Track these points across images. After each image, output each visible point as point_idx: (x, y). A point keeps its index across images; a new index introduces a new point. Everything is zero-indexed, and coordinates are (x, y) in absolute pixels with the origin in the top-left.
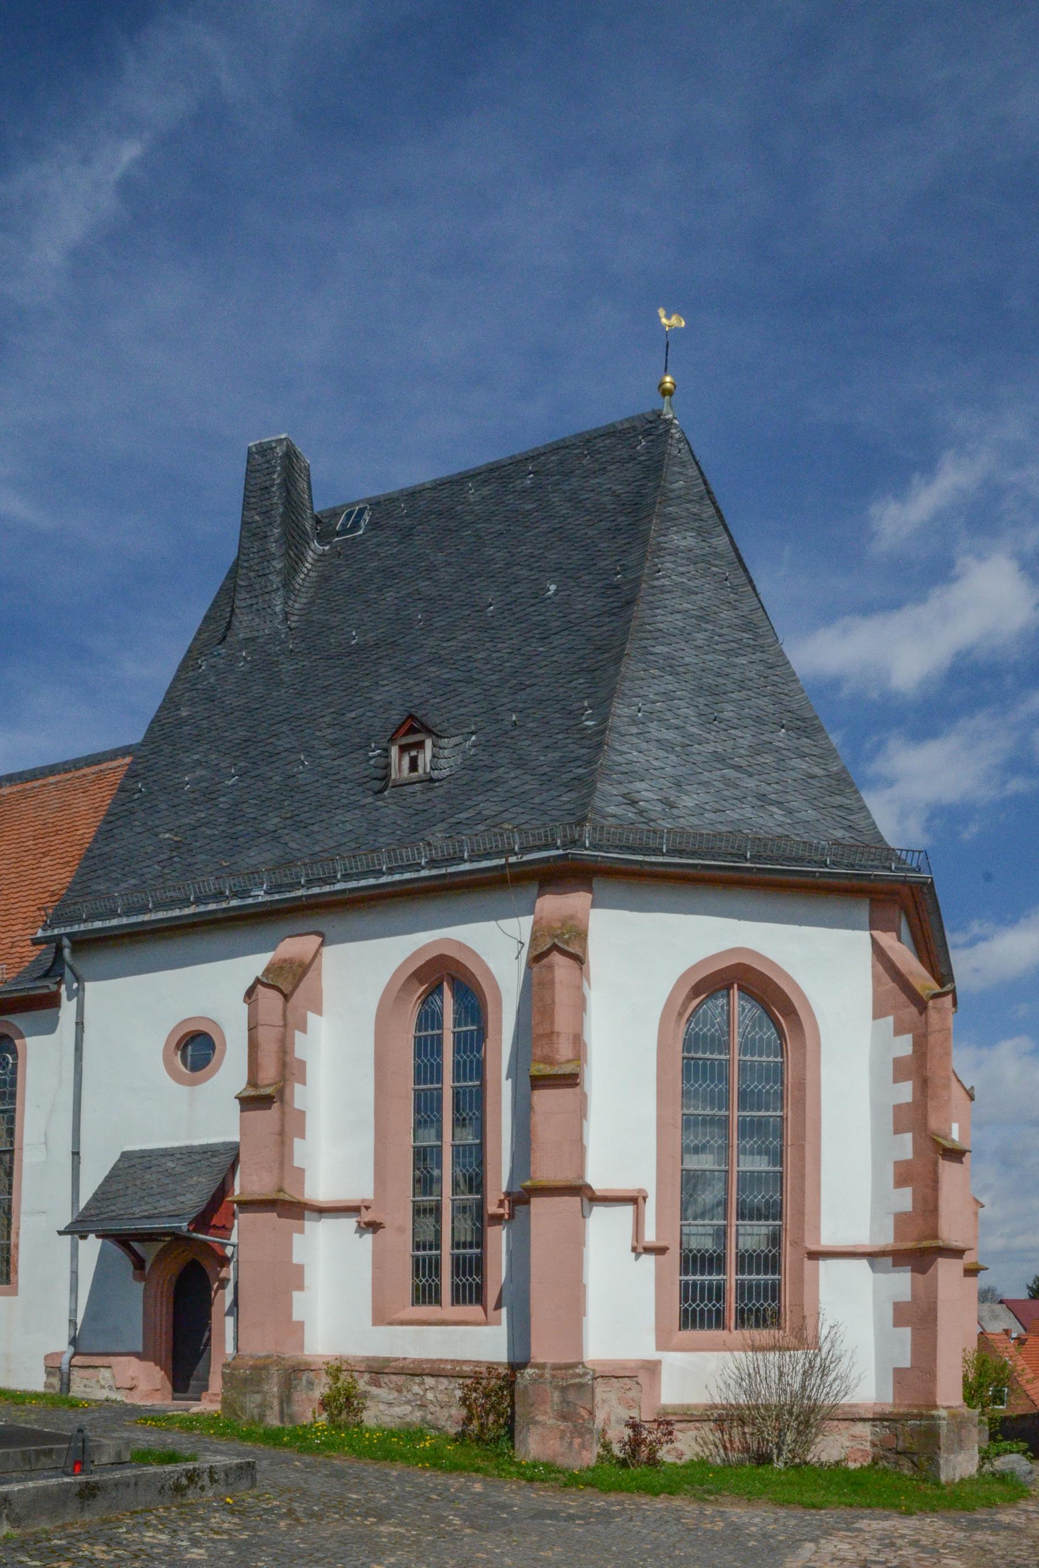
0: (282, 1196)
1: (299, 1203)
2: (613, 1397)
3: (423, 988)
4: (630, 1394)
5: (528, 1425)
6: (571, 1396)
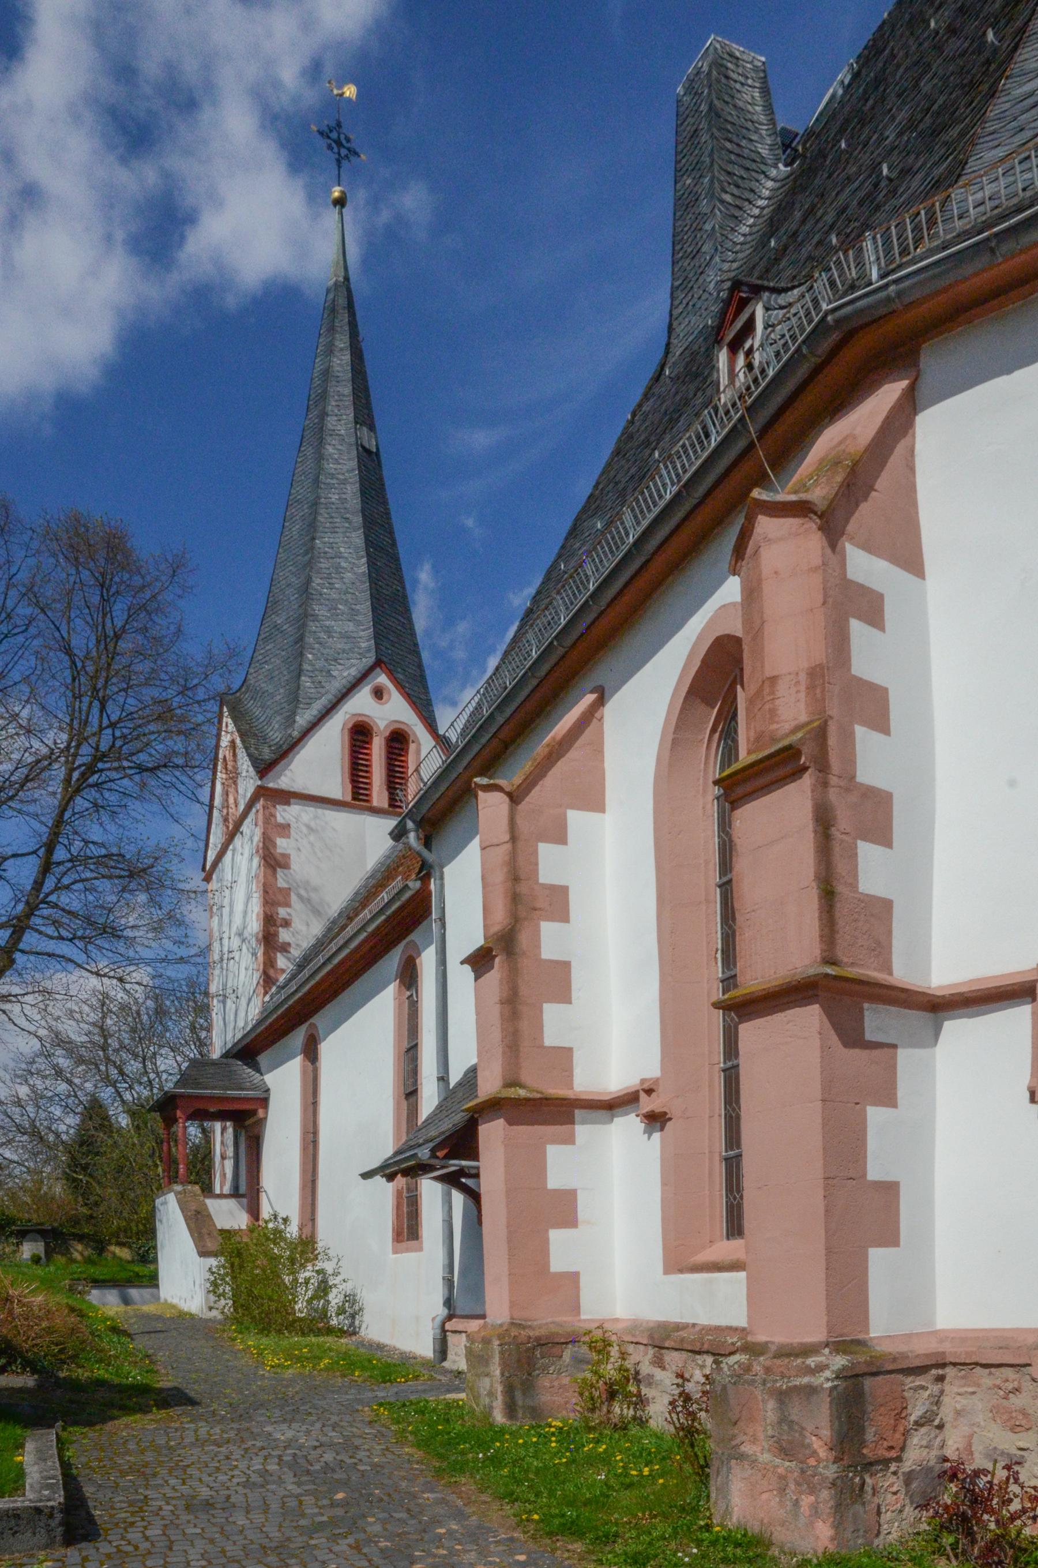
1: (546, 1099)
2: (978, 1405)
4: (1016, 1401)
5: (729, 1460)
6: (795, 1412)
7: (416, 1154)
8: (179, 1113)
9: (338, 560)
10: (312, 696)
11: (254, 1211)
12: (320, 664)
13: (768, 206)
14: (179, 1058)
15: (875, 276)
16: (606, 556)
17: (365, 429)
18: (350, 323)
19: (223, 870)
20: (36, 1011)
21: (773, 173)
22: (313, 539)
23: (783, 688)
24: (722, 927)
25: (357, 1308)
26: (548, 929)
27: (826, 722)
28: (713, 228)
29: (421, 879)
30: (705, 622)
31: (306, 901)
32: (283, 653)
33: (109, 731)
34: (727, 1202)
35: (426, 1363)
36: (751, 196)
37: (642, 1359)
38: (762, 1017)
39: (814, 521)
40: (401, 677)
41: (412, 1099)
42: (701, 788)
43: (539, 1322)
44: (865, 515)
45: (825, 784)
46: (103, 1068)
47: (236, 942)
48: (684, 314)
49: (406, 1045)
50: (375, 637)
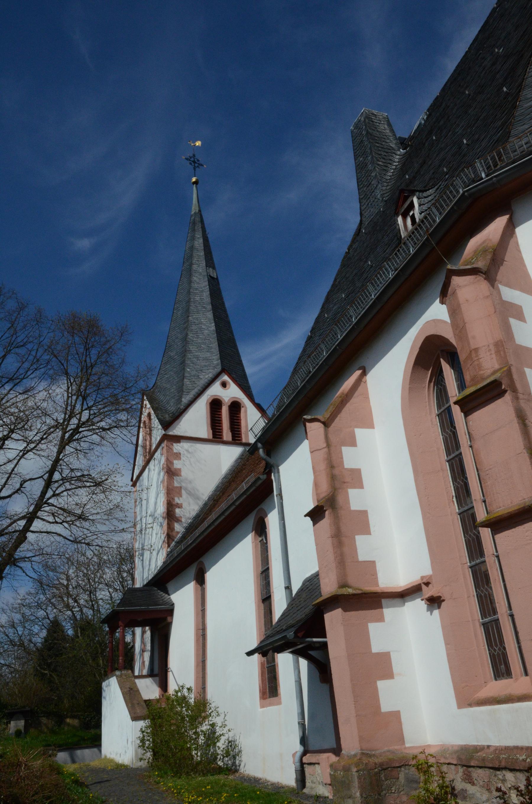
1: (365, 594)
3: (430, 371)
7: (286, 636)
8: (120, 623)
9: (201, 325)
10: (190, 388)
11: (164, 685)
12: (194, 373)
13: (399, 165)
14: (111, 590)
15: (483, 175)
16: (360, 305)
17: (211, 269)
18: (202, 227)
19: (143, 480)
20: (40, 567)
21: (399, 153)
22: (188, 317)
23: (482, 354)
24: (453, 484)
25: (237, 751)
26: (353, 493)
27: (510, 368)
28: (376, 174)
29: (267, 474)
30: (418, 331)
31: (190, 494)
32: (175, 369)
33: (87, 411)
34: (490, 654)
35: (291, 791)
36: (390, 162)
37: (456, 777)
38: (509, 529)
39: (481, 276)
40: (234, 376)
41: (267, 603)
42: (428, 411)
43: (377, 752)
44: (503, 272)
45: (517, 398)
46: (65, 599)
47: (150, 520)
48: (367, 208)
49: (260, 569)
50: (221, 359)
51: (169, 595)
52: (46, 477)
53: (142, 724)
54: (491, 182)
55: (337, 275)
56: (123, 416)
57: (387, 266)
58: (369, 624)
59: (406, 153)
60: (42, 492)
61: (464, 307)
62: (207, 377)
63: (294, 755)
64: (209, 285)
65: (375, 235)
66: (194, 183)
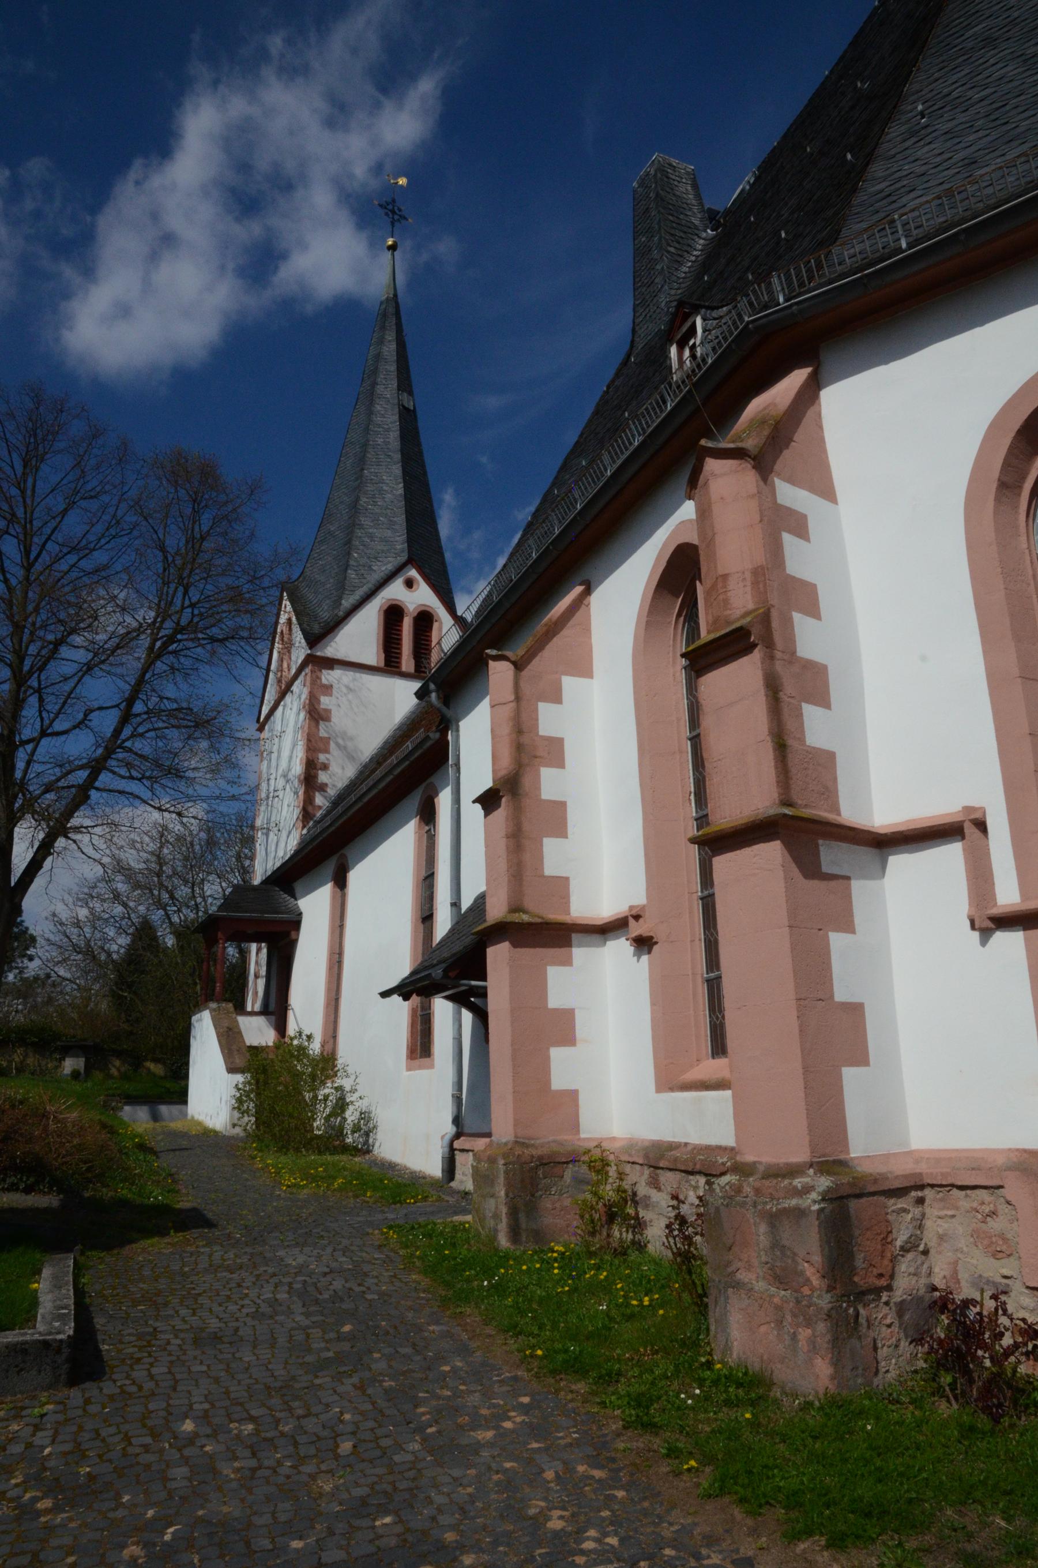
0: (517, 918)
1: (547, 924)
2: (959, 1229)
4: (995, 1225)
8: (220, 935)
11: (281, 1027)
12: (362, 561)
17: (405, 394)
18: (396, 324)
20: (102, 841)
21: (704, 235)
22: (363, 469)
23: (732, 583)
25: (371, 1126)
26: (547, 774)
27: (769, 609)
33: (189, 610)
35: (434, 1183)
36: (689, 249)
37: (638, 1179)
41: (428, 923)
45: (772, 658)
46: (156, 892)
47: (281, 782)
49: (424, 874)
51: (296, 899)
52: (122, 706)
53: (239, 1078)
54: (789, 311)
55: (586, 427)
56: (245, 620)
57: (633, 427)
58: (549, 968)
59: (716, 236)
60: (115, 730)
61: (717, 509)
62: (383, 569)
63: (443, 1137)
64: (400, 420)
65: (642, 367)
66: (390, 248)
